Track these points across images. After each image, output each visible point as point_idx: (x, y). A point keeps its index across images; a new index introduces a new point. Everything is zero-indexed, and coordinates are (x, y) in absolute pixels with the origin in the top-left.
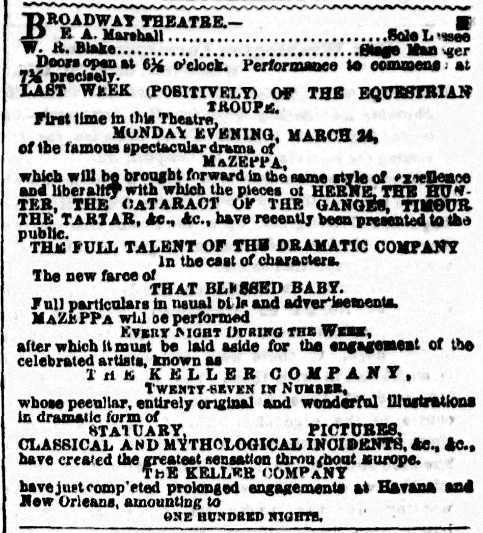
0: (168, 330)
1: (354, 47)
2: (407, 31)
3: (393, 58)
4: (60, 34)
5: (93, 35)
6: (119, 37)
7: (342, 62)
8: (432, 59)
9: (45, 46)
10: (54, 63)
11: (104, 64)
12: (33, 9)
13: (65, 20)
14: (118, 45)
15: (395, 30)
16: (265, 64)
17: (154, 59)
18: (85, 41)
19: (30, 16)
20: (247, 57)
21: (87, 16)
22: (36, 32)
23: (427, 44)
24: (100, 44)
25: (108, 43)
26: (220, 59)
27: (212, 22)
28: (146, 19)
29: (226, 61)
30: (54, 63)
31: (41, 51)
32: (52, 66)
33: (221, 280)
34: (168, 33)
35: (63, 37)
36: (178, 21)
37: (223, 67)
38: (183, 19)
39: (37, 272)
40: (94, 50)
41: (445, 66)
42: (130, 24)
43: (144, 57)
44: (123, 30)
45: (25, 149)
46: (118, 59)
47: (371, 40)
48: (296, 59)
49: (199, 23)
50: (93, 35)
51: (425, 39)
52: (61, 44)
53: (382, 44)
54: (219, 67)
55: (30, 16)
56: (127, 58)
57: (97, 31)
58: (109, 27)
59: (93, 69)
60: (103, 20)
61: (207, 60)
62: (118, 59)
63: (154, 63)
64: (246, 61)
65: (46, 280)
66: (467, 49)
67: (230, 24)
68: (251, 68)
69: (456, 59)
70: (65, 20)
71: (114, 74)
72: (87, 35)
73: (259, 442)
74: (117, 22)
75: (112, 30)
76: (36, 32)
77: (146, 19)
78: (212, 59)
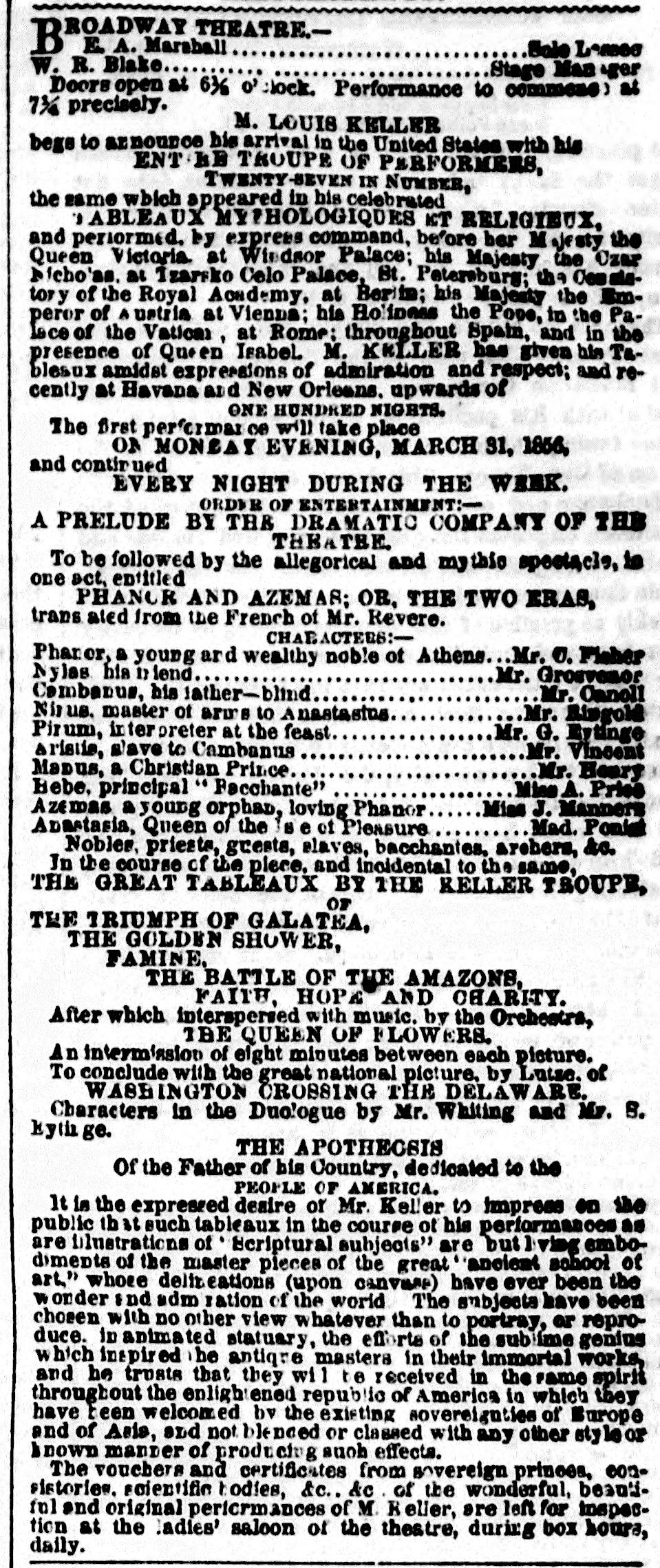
0: (252, 604)
1: (484, 65)
2: (555, 43)
3: (536, 81)
4: (83, 45)
6: (167, 48)
7: (468, 86)
8: (587, 81)
9: (63, 64)
10: (74, 86)
11: (144, 85)
12: (44, 14)
13: (90, 26)
14: (167, 59)
16: (366, 87)
17: (215, 78)
18: (118, 55)
19: (41, 23)
20: (339, 77)
21: (121, 20)
22: (50, 44)
23: (582, 61)
24: (141, 58)
25: (151, 57)
26: (305, 80)
27: (290, 29)
28: (201, 24)
29: (312, 86)
30: (74, 86)
31: (56, 70)
32: (72, 91)
33: (102, 400)
34: (232, 43)
35: (86, 51)
36: (244, 28)
37: (309, 90)
38: (250, 25)
39: (55, 421)
40: (130, 67)
42: (180, 31)
43: (200, 75)
44: (172, 38)
46: (166, 78)
47: (505, 55)
48: (406, 80)
49: (272, 31)
50: (130, 46)
51: (580, 54)
52: (85, 60)
53: (521, 62)
54: (303, 89)
55: (41, 23)
56: (178, 76)
58: (153, 35)
59: (129, 93)
60: (144, 24)
61: (287, 81)
62: (166, 78)
63: (215, 83)
64: (339, 82)
65: (67, 432)
66: (637, 66)
67: (315, 31)
68: (347, 91)
69: (621, 79)
70: (90, 26)
71: (159, 100)
72: (122, 46)
73: (257, 481)
74: (164, 29)
76: (50, 44)
77: (201, 24)
78: (292, 79)
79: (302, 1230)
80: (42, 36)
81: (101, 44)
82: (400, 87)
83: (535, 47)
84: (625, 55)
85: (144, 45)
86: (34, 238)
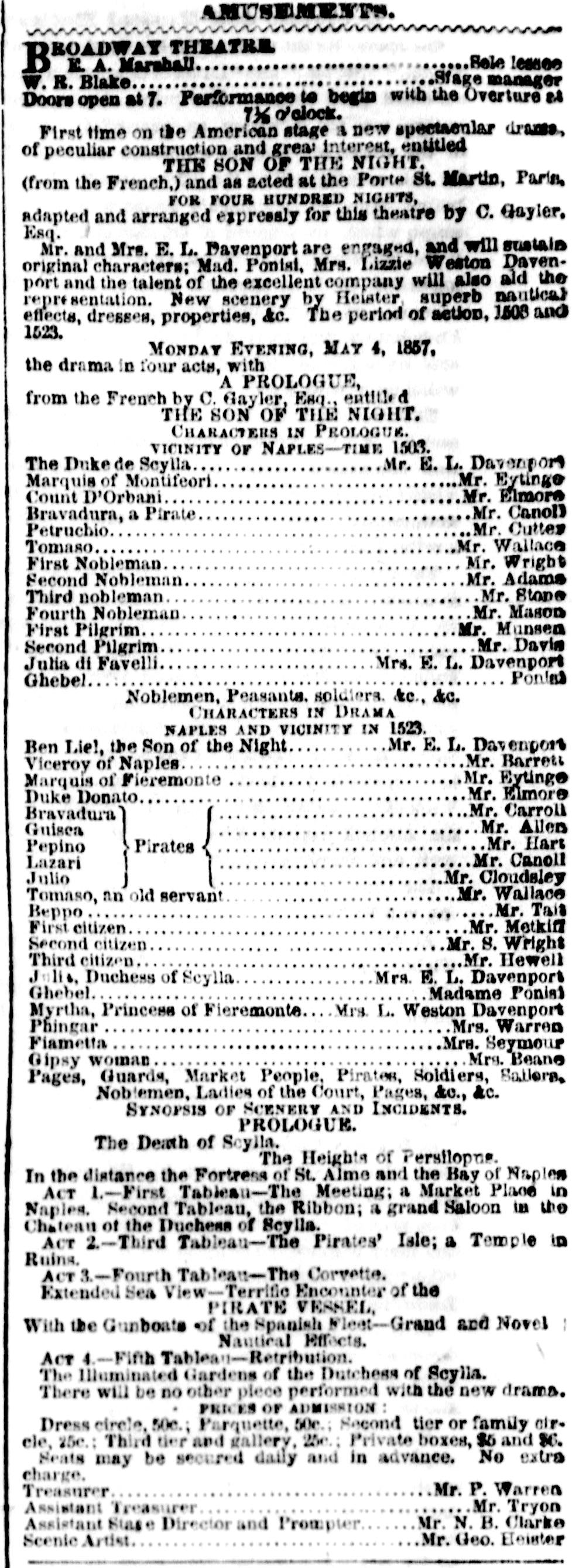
5: (107, 66)
6: (141, 68)
12: (37, 38)
14: (135, 78)
15: (437, 1367)
22: (39, 64)
28: (175, 44)
34: (201, 60)
38: (221, 43)
41: (556, 465)
42: (155, 52)
44: (143, 59)
45: (29, 150)
49: (240, 48)
56: (308, 90)
57: (112, 61)
60: (121, 47)
70: (73, 49)
72: (100, 67)
75: (131, 59)
76: (39, 64)
79: (172, 751)
80: (31, 57)
81: (82, 65)
82: (239, 95)
83: (477, 61)
84: (529, 69)
85: (118, 65)
86: (26, 216)
